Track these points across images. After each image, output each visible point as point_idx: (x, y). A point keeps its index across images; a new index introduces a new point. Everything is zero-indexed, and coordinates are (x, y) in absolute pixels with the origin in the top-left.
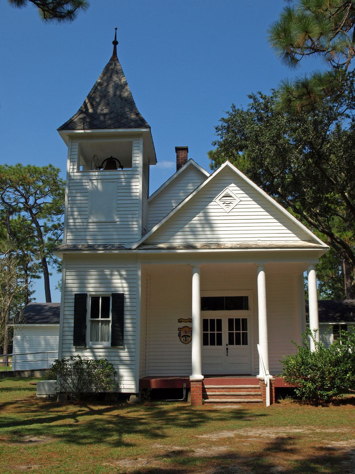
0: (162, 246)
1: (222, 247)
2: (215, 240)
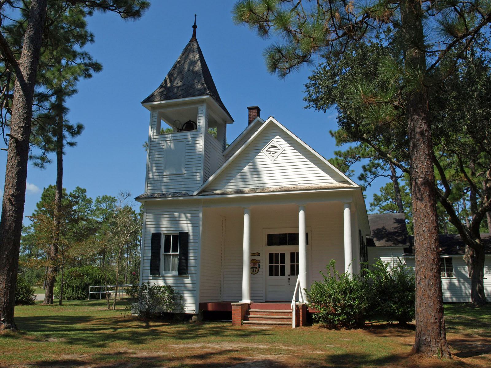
0: (218, 192)
1: (266, 191)
2: (261, 185)
